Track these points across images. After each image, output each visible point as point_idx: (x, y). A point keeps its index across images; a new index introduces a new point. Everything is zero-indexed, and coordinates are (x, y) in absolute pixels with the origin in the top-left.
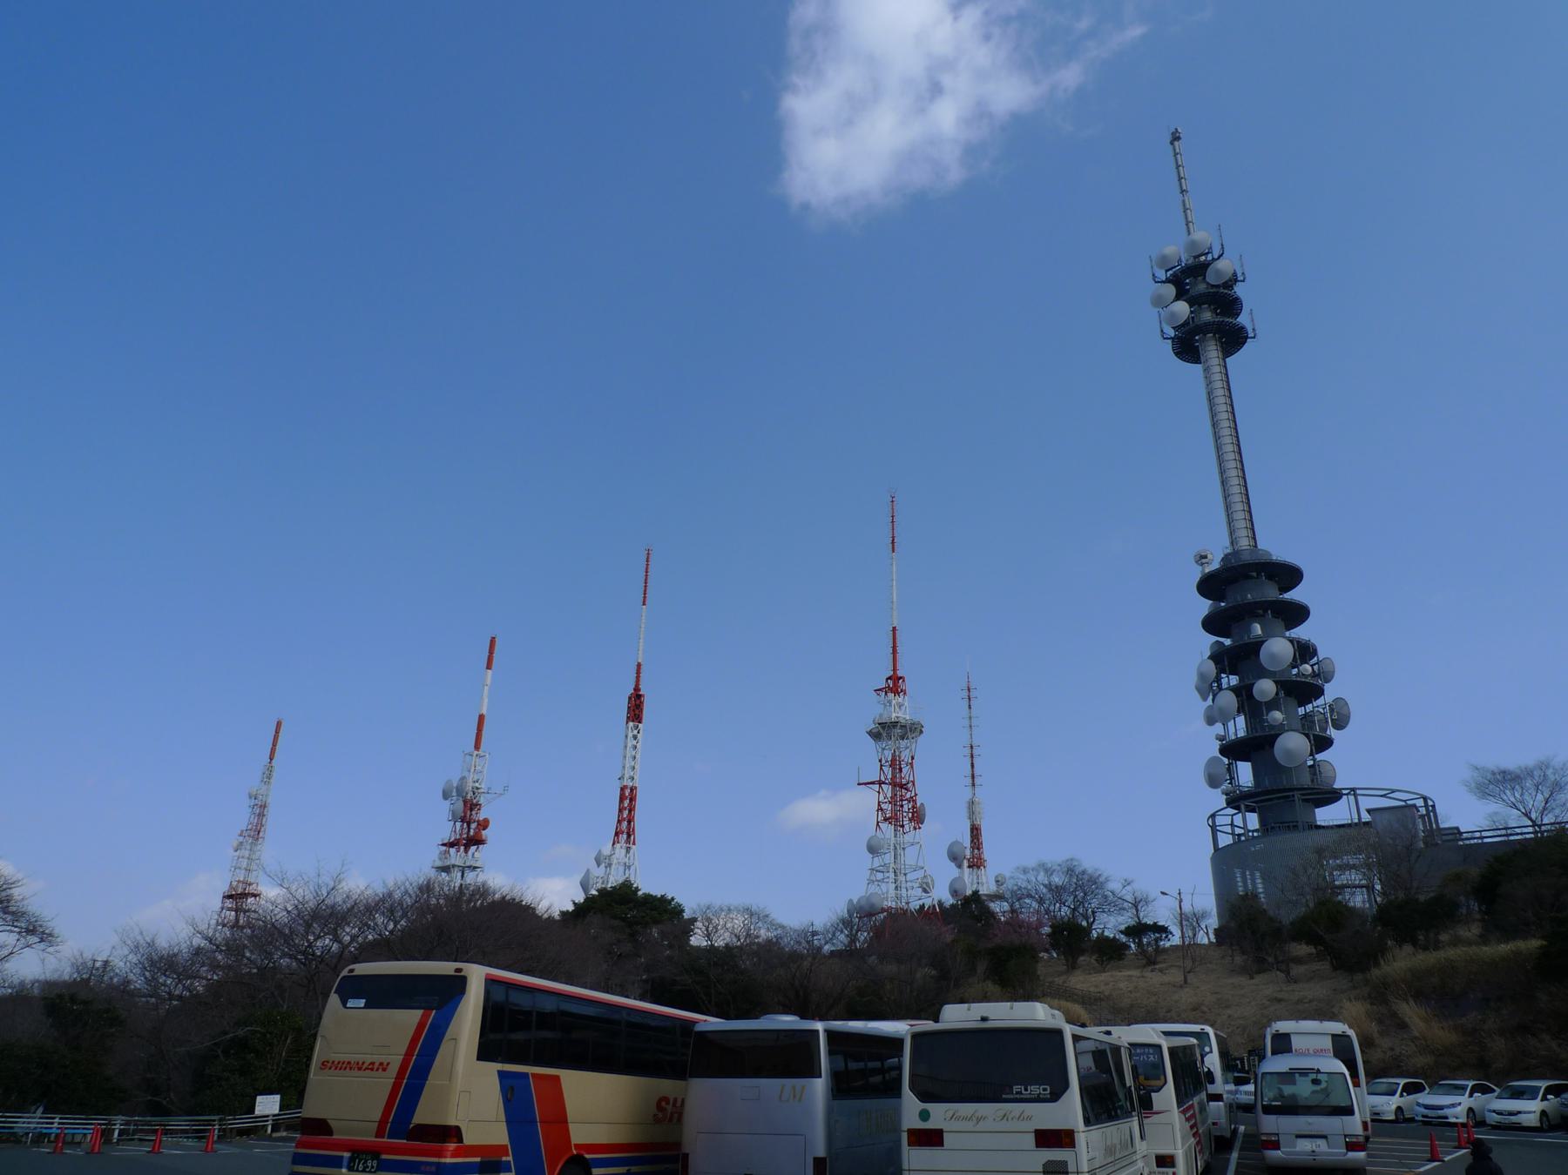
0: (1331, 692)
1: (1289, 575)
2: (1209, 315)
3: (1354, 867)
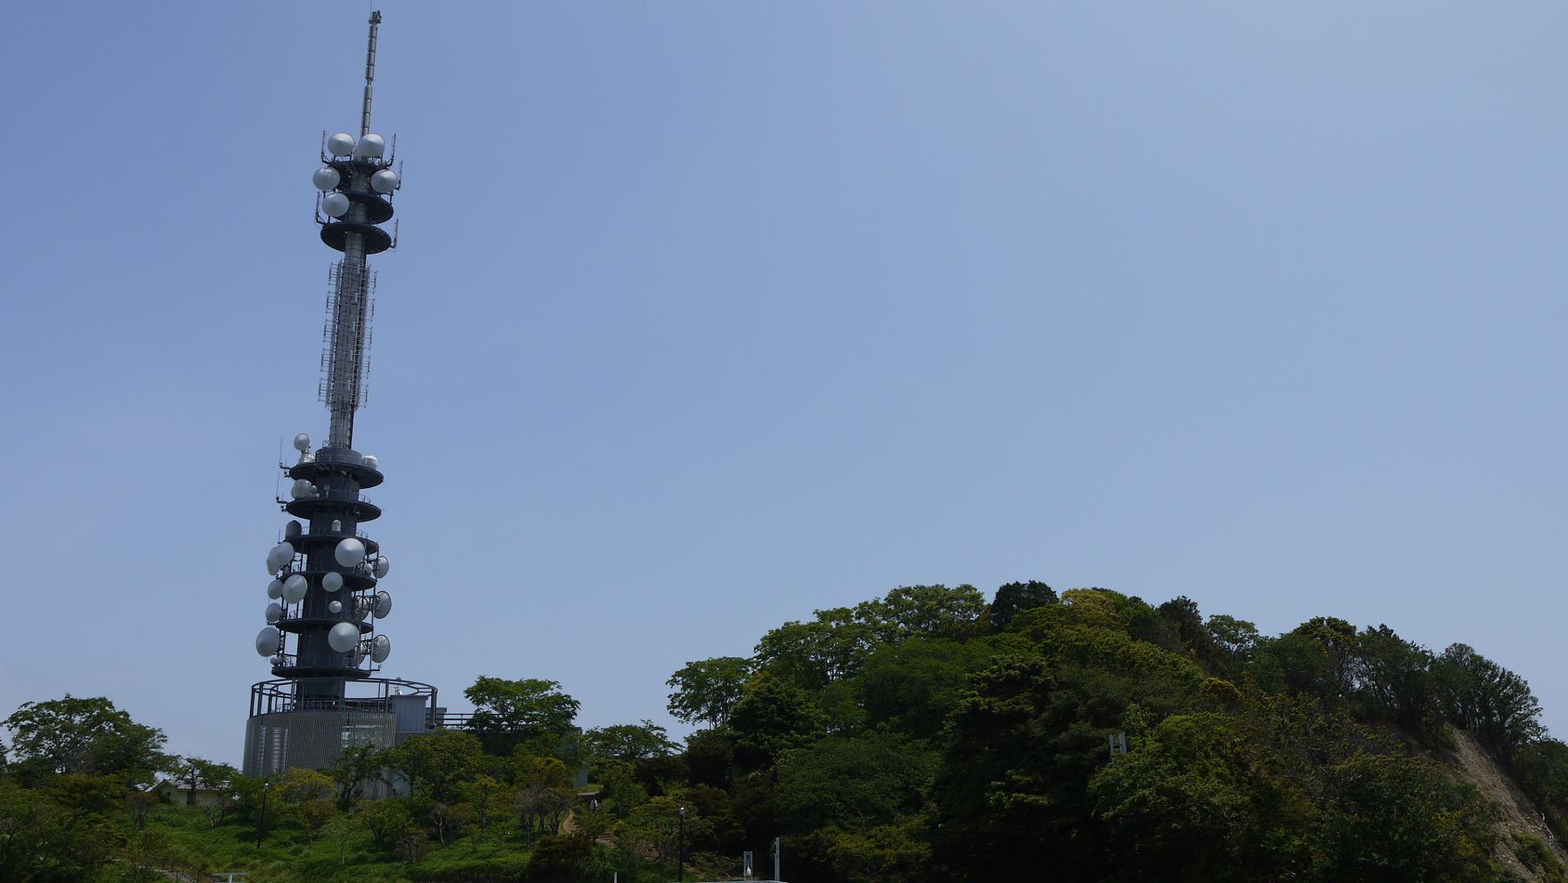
0: (382, 585)
1: (372, 478)
2: (359, 211)
3: (648, 868)
